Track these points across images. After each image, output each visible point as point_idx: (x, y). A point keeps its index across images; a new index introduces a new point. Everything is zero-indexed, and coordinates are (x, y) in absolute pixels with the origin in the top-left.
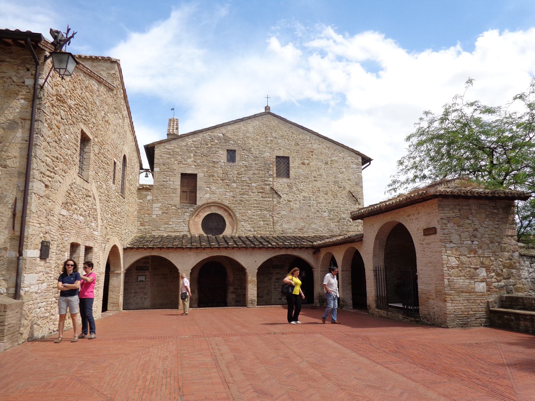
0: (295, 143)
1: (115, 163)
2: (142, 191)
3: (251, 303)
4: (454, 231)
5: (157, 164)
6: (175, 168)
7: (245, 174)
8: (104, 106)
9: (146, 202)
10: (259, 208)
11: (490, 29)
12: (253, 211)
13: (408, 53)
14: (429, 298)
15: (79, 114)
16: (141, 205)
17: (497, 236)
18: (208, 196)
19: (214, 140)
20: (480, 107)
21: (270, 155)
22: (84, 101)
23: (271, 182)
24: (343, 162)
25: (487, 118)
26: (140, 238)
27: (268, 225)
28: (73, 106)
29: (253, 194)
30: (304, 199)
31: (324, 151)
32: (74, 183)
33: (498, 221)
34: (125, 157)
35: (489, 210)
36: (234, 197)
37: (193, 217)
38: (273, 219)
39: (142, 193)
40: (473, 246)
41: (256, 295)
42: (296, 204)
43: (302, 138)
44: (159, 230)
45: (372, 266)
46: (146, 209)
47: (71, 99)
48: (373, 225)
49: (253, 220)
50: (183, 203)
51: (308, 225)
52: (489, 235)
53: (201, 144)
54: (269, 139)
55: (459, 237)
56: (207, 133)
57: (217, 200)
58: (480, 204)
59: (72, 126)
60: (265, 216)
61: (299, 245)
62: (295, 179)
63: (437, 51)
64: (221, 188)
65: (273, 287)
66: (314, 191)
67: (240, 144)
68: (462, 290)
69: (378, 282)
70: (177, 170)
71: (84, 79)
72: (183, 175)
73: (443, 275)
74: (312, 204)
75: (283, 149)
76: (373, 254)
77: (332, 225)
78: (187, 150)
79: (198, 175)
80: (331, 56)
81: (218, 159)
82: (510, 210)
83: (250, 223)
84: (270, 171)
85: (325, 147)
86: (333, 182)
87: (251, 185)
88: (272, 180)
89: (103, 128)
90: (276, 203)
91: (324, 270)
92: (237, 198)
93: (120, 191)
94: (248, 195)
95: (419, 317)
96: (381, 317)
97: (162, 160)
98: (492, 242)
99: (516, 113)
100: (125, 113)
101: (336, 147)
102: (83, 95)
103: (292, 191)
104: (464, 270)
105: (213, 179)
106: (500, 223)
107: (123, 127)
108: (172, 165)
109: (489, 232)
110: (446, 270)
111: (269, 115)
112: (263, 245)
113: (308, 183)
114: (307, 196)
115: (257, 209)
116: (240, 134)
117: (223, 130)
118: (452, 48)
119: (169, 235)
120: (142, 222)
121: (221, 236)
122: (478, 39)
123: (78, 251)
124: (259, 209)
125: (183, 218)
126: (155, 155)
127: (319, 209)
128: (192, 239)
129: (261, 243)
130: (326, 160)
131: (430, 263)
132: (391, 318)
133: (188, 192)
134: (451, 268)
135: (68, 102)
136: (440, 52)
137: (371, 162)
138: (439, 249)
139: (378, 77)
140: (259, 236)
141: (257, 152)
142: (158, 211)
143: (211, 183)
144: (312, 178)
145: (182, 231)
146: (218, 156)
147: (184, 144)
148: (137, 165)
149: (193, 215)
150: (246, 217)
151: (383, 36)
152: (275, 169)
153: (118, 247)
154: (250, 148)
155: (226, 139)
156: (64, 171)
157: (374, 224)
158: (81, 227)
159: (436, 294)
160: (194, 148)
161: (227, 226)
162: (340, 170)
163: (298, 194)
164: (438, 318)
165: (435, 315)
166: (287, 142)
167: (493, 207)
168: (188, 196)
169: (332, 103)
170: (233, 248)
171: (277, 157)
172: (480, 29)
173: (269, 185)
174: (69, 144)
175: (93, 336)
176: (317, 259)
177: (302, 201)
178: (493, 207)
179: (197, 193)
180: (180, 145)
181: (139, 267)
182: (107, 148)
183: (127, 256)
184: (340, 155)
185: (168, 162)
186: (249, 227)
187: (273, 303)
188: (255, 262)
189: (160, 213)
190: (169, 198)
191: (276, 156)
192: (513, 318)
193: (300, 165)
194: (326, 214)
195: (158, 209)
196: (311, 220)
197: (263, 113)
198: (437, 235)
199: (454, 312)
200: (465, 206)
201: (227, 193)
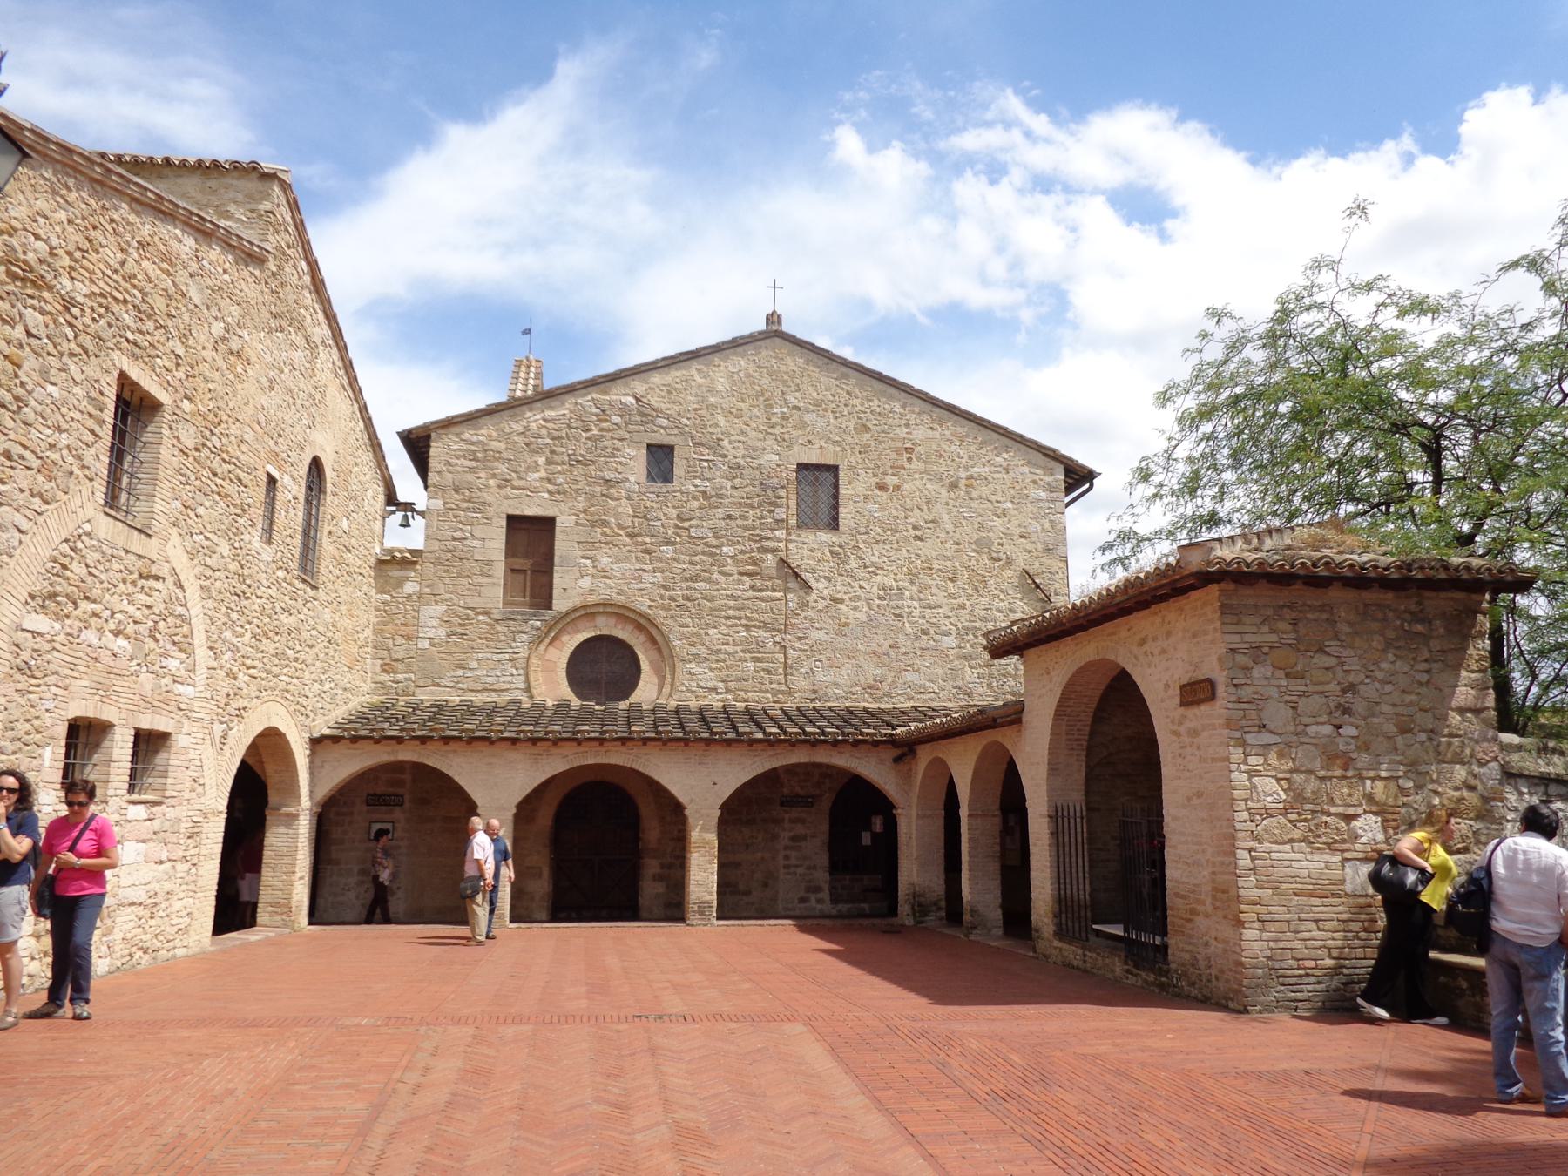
1: (272, 481)
2: (388, 567)
4: (1273, 692)
6: (489, 499)
7: (700, 518)
8: (222, 304)
10: (744, 622)
11: (1503, 84)
12: (724, 629)
13: (1254, 162)
14: (1194, 912)
15: (110, 325)
17: (1426, 711)
18: (586, 583)
20: (1394, 294)
21: (778, 460)
22: (135, 286)
23: (780, 541)
25: (1424, 333)
26: (377, 708)
27: (769, 672)
28: (80, 299)
30: (882, 593)
32: (88, 534)
33: (1426, 661)
34: (316, 465)
35: (1398, 622)
36: (666, 588)
37: (542, 647)
38: (785, 654)
40: (1340, 741)
41: (715, 888)
42: (855, 609)
43: (878, 410)
44: (438, 685)
47: (72, 278)
48: (1048, 673)
49: (722, 656)
50: (512, 604)
52: (1394, 705)
53: (569, 427)
55: (1291, 711)
57: (614, 595)
58: (1366, 605)
59: (76, 359)
61: (848, 734)
63: (1344, 156)
64: (627, 560)
65: (782, 862)
66: (914, 571)
68: (1299, 886)
71: (132, 218)
72: (516, 523)
73: (1233, 837)
75: (818, 443)
78: (527, 445)
80: (1017, 176)
82: (1474, 626)
83: (715, 665)
84: (777, 510)
85: (950, 437)
86: (975, 543)
89: (218, 374)
91: (929, 813)
93: (294, 565)
94: (709, 581)
95: (1166, 973)
97: (450, 476)
98: (1404, 730)
99: (1511, 311)
100: (321, 331)
101: (982, 436)
102: (130, 266)
104: (1305, 820)
105: (604, 534)
106: (1436, 666)
108: (479, 489)
109: (1396, 698)
110: (1245, 821)
111: (777, 339)
113: (895, 546)
115: (736, 626)
116: (689, 398)
117: (639, 386)
118: (1389, 145)
120: (387, 661)
121: (623, 705)
122: (1468, 115)
123: (106, 744)
126: (431, 460)
127: (928, 626)
128: (539, 714)
131: (1198, 797)
132: (1095, 971)
134: (1261, 815)
135: (59, 287)
136: (1352, 157)
137: (1095, 481)
138: (1222, 752)
139: (1163, 236)
141: (741, 453)
144: (907, 531)
145: (506, 690)
146: (621, 463)
147: (518, 427)
148: (376, 494)
150: (703, 649)
151: (1174, 113)
152: (793, 503)
154: (718, 439)
155: (646, 413)
156: (40, 495)
158: (115, 671)
159: (1214, 897)
163: (863, 579)
164: (1217, 978)
165: (1210, 967)
166: (832, 421)
167: (1411, 613)
169: (1027, 315)
170: (646, 741)
171: (802, 467)
172: (1473, 88)
173: (774, 551)
174: (63, 416)
175: (82, 1009)
177: (877, 601)
178: (1411, 613)
179: (555, 575)
180: (507, 430)
181: (375, 795)
182: (239, 432)
184: (998, 459)
185: (468, 483)
186: (710, 679)
189: (442, 633)
191: (799, 465)
192: (1465, 985)
194: (949, 641)
195: (435, 623)
196: (902, 658)
197: (760, 333)
198: (1219, 703)
199: (1269, 958)
200: (1312, 608)
201: (645, 575)
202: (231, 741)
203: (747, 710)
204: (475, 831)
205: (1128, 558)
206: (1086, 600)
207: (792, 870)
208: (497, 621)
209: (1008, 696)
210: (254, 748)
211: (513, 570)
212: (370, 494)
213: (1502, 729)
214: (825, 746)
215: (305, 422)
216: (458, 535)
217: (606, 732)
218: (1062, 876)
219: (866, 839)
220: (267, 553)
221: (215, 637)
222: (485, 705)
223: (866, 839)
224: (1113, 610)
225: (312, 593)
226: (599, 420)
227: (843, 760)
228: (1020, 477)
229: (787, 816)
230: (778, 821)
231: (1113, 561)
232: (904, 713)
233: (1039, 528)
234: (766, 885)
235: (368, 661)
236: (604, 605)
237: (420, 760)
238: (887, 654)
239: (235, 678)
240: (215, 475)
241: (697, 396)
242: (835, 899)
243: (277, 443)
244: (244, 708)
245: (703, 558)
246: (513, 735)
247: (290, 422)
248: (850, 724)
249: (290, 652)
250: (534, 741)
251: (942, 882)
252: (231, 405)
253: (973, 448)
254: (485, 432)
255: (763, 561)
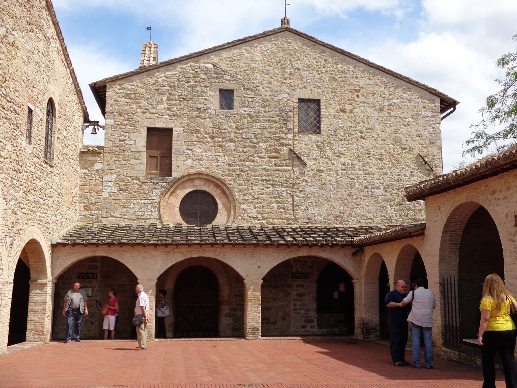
0: (330, 77)
1: (30, 111)
2: (87, 155)
3: (252, 333)
5: (109, 113)
6: (138, 119)
7: (248, 128)
8: (4, 18)
9: (93, 172)
10: (271, 182)
12: (261, 186)
16: (85, 178)
18: (189, 163)
19: (199, 74)
23: (290, 140)
24: (410, 107)
26: (83, 228)
27: (284, 209)
29: (261, 160)
30: (343, 167)
31: (378, 90)
34: (51, 102)
36: (230, 165)
37: (167, 196)
38: (293, 199)
39: (87, 159)
41: (260, 321)
42: (330, 175)
43: (341, 69)
44: (113, 217)
45: (438, 277)
46: (93, 184)
49: (260, 201)
50: (151, 174)
51: (349, 209)
53: (179, 81)
54: (287, 70)
56: (189, 62)
57: (204, 169)
60: (280, 194)
61: (329, 241)
62: (329, 135)
64: (210, 150)
66: (360, 155)
67: (240, 81)
69: (446, 302)
70: (141, 122)
72: (150, 130)
74: (356, 176)
75: (309, 87)
76: (440, 256)
77: (390, 210)
78: (157, 90)
79: (174, 130)
81: (205, 105)
83: (257, 205)
85: (379, 83)
86: (393, 140)
87: (257, 146)
88: (292, 137)
89: (4, 55)
90: (298, 173)
91: (370, 282)
92: (235, 166)
93: (42, 155)
94: (253, 161)
96: (451, 360)
100: (51, 31)
103: (324, 155)
105: (198, 137)
107: (46, 54)
108: (132, 114)
111: (287, 32)
112: (271, 240)
113: (351, 142)
114: (348, 163)
115: (267, 184)
117: (214, 58)
119: (128, 224)
120: (87, 204)
121: (209, 226)
124: (271, 185)
125: (150, 198)
129: (269, 237)
130: (381, 105)
133: (159, 157)
137: (457, 106)
140: (270, 226)
141: (269, 93)
142: (111, 187)
143: (194, 143)
144: (356, 134)
145: (149, 219)
146: (206, 99)
147: (152, 81)
149: (166, 194)
150: (250, 197)
152: (296, 120)
153: (39, 243)
154: (257, 86)
155: (219, 73)
157: (441, 206)
160: (168, 88)
161: (219, 211)
162: (405, 119)
168: (159, 163)
169: (399, 13)
170: (224, 245)
171: (301, 100)
173: (287, 145)
176: (359, 264)
177: (341, 171)
179: (173, 159)
180: (146, 83)
181: (82, 273)
182: (14, 86)
183: (58, 256)
184: (405, 95)
186: (254, 212)
187: (293, 333)
188: (259, 267)
189: (115, 189)
190: (128, 167)
191: (299, 99)
193: (338, 113)
195: (111, 184)
196: (354, 201)
197: (278, 29)
201: (220, 159)
202: (15, 246)
203: (274, 228)
204: (140, 292)
205: (481, 147)
206: (463, 171)
207: (298, 311)
208: (143, 183)
209: (410, 221)
210: (24, 251)
211: (151, 157)
212: (76, 117)
213: (425, 223)
214: (338, 247)
215: (45, 80)
216: (122, 138)
217: (203, 240)
218: (447, 314)
219: (336, 295)
220: (29, 149)
221: (6, 193)
222: (139, 226)
223: (336, 295)
224: (479, 176)
225: (50, 169)
226: (193, 77)
227: (325, 254)
228: (417, 104)
229: (294, 284)
230: (291, 286)
231: (474, 148)
232: (356, 230)
233: (427, 132)
234: (284, 319)
235: (77, 204)
236: (199, 174)
237: (108, 256)
238: (347, 199)
239: (16, 214)
240: (4, 108)
241: (245, 63)
242: (320, 326)
243: (32, 91)
244: (21, 229)
245: (250, 149)
246: (155, 242)
247: (38, 80)
248: (329, 236)
249: (41, 200)
250: (166, 245)
251: (378, 318)
252: (10, 71)
253: (391, 89)
254: (135, 83)
255: (281, 151)
